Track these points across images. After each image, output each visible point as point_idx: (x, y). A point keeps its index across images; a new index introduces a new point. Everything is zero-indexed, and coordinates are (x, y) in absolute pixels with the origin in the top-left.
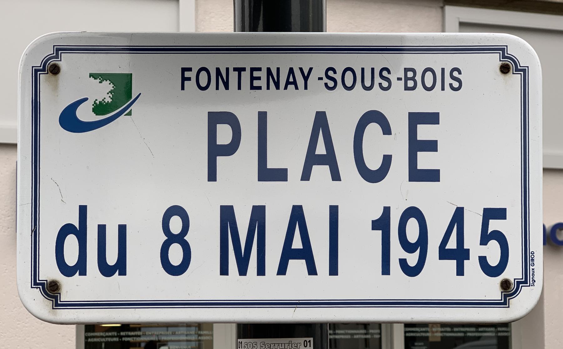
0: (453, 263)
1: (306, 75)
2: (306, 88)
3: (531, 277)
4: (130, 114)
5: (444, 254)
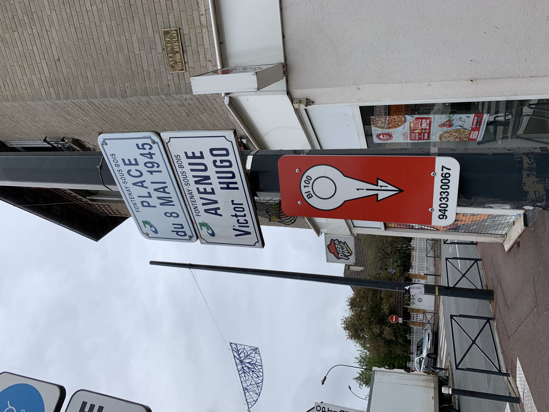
5: (152, 158)
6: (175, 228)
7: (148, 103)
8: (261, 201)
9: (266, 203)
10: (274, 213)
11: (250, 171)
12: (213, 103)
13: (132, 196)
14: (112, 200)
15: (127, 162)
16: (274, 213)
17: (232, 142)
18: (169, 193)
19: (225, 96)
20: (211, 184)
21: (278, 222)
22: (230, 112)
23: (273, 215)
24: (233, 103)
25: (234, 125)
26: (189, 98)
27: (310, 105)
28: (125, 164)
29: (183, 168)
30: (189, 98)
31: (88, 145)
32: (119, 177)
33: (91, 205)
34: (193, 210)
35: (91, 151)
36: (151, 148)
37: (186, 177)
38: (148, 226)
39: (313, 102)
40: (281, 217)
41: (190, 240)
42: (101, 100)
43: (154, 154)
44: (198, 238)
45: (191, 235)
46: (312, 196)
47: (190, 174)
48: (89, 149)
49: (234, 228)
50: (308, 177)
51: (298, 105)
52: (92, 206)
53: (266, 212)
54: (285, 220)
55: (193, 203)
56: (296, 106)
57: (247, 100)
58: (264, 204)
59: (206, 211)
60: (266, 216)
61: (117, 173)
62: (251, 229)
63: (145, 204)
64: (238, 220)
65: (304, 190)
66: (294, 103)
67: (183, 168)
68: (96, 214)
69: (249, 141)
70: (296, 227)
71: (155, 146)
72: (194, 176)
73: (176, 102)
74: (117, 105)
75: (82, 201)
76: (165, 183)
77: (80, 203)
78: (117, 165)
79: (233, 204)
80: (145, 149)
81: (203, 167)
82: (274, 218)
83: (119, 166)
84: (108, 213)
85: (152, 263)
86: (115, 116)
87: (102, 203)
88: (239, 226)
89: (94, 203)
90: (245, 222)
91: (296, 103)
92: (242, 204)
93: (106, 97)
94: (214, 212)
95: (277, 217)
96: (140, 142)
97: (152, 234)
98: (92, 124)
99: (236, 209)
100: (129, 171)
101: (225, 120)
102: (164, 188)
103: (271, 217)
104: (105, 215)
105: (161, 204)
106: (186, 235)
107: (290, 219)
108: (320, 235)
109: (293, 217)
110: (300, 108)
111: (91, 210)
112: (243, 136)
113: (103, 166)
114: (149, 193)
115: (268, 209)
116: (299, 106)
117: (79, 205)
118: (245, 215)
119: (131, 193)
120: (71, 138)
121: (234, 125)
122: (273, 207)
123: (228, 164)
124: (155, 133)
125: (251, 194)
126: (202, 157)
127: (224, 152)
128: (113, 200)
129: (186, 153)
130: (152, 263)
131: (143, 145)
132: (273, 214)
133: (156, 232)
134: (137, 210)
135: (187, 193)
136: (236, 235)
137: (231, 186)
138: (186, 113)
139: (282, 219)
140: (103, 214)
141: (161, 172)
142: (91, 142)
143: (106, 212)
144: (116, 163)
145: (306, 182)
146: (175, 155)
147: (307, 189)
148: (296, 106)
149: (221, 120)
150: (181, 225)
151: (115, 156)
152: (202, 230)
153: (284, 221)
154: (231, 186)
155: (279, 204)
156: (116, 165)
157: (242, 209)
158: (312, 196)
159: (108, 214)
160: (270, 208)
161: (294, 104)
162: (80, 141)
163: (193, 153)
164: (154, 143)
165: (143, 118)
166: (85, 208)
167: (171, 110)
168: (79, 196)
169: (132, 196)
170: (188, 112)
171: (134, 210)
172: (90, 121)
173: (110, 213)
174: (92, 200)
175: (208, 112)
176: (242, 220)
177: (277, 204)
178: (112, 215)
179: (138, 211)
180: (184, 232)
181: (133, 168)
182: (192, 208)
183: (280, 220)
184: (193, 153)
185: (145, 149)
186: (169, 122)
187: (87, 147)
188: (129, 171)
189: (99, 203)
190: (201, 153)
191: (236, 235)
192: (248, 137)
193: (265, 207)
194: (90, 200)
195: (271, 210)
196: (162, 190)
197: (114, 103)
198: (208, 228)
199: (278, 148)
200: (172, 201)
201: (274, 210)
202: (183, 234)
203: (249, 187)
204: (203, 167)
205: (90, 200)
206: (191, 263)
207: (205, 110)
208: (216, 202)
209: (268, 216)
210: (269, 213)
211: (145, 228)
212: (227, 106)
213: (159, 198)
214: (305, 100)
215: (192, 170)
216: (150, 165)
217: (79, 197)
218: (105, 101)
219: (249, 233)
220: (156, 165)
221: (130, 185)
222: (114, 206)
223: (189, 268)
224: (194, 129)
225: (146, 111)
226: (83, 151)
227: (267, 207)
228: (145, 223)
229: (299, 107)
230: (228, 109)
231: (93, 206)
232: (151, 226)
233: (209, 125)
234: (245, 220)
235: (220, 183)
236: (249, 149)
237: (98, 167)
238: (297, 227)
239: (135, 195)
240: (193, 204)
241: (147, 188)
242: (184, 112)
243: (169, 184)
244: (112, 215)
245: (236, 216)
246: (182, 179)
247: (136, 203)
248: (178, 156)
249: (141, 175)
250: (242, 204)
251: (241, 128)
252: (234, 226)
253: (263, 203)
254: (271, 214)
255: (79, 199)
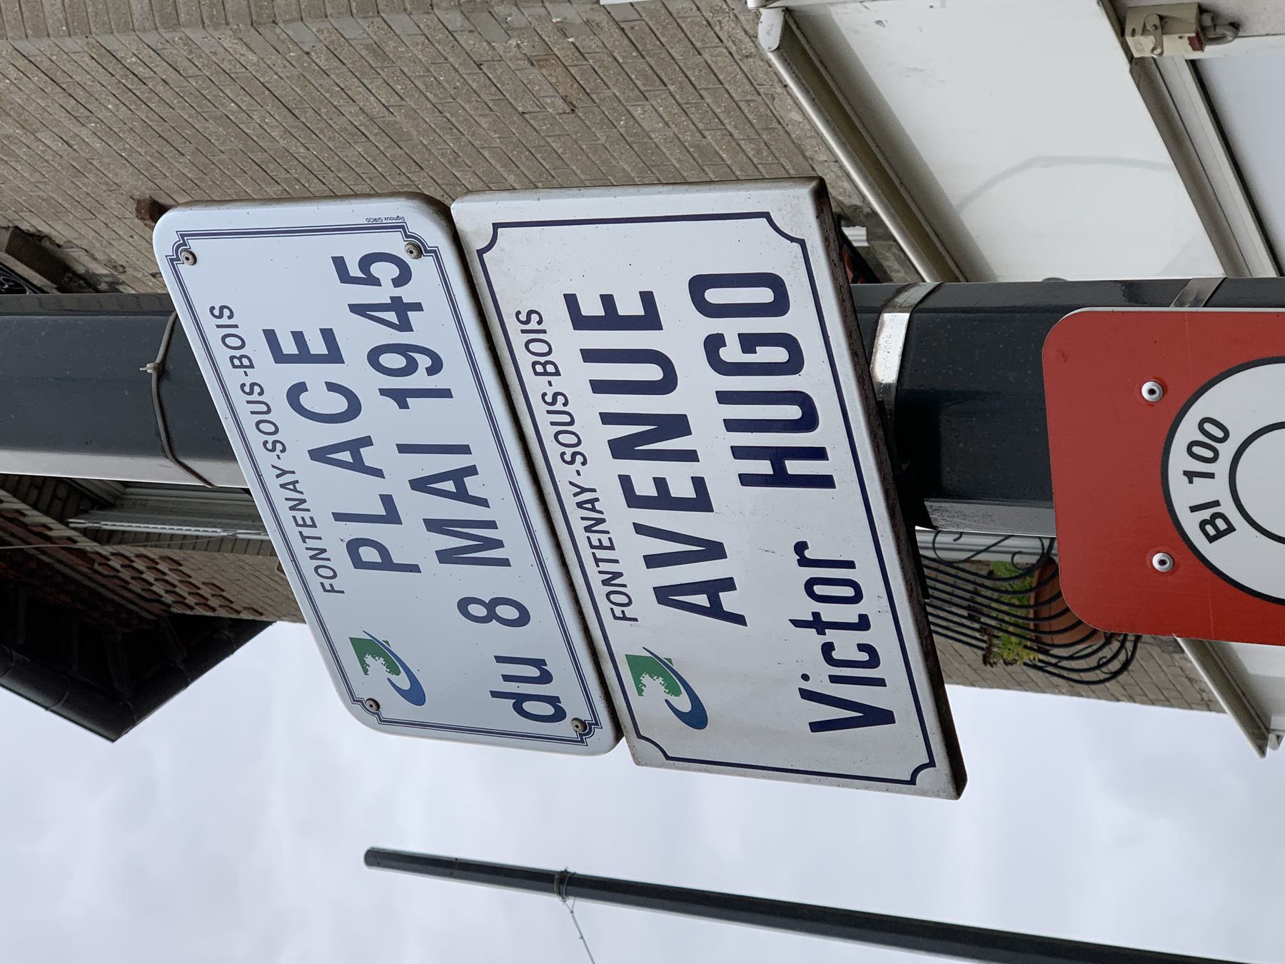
0: (412, 315)
1: (580, 490)
2: (594, 490)
3: (394, 221)
4: (669, 660)
5: (405, 326)
6: (507, 678)
7: (377, 49)
8: (943, 555)
9: (966, 566)
10: (1013, 620)
11: (894, 390)
12: (698, 45)
13: (306, 515)
14: (192, 537)
15: (289, 347)
16: (1013, 620)
17: (802, 243)
18: (483, 502)
19: (764, 6)
20: (691, 456)
21: (1034, 667)
22: (786, 86)
23: (1007, 632)
24: (803, 41)
25: (804, 156)
26: (578, 21)
27: (1219, 39)
28: (279, 357)
29: (557, 373)
30: (578, 21)
31: (85, 259)
32: (248, 422)
33: (93, 556)
34: (600, 591)
35: (97, 291)
36: (404, 277)
37: (567, 419)
38: (376, 664)
39: (1235, 26)
40: (1047, 639)
41: (582, 741)
42: (152, 38)
43: (417, 307)
44: (619, 733)
45: (586, 716)
46: (1231, 529)
47: (586, 407)
48: (88, 283)
49: (807, 686)
50: (1208, 426)
51: (1152, 38)
52: (94, 561)
53: (965, 613)
54: (1071, 658)
55: (601, 554)
56: (1143, 46)
57: (879, 22)
58: (953, 571)
59: (665, 595)
60: (969, 632)
61: (239, 399)
62: (893, 696)
63: (368, 554)
64: (827, 649)
65: (1183, 495)
66: (1128, 30)
67: (557, 373)
68: (112, 601)
69: (880, 238)
70: (1131, 699)
71: (422, 268)
72: (608, 418)
73: (513, 42)
74: (226, 66)
75: (49, 539)
76: (465, 450)
77: (37, 549)
78: (240, 358)
79: (804, 562)
80: (375, 282)
81: (653, 373)
82: (1009, 646)
83: (251, 366)
84: (168, 599)
85: (377, 858)
86: (215, 119)
87: (142, 550)
88: (834, 679)
89: (106, 550)
90: (864, 657)
91: (1139, 30)
92: (850, 565)
93: (173, 22)
94: (702, 600)
95: (1029, 644)
96: (354, 249)
97: (395, 706)
98: (107, 160)
99: (819, 590)
100: (295, 392)
101: (757, 127)
102: (458, 476)
103: (996, 641)
104: (155, 608)
105: (446, 556)
106: (559, 715)
107: (1100, 654)
108: (1269, 750)
109: (1115, 645)
110: (1161, 54)
111: (92, 585)
112: (848, 212)
113: (170, 366)
114: (387, 500)
115: (979, 599)
116: (1159, 44)
117: (31, 557)
118: (863, 623)
119: (304, 501)
120: (7, 228)
121: (804, 156)
122: (1005, 585)
123: (779, 355)
124: (423, 206)
125: (898, 508)
126: (650, 319)
127: (764, 295)
128: (197, 537)
129: (571, 301)
130: (377, 858)
131: (366, 262)
132: (1004, 626)
133: (415, 695)
134: (327, 583)
135: (570, 502)
136: (817, 727)
137: (794, 467)
138: (564, 99)
139: (1055, 651)
140: (147, 605)
141: (446, 393)
142: (97, 245)
143: (162, 593)
144: (238, 353)
145: (1196, 450)
146: (518, 313)
147: (1203, 491)
148: (1143, 46)
149: (736, 127)
150: (539, 663)
151: (231, 317)
152: (640, 692)
153: (1064, 663)
154: (794, 467)
155: (1036, 574)
156: (237, 362)
157: (848, 592)
158: (1231, 529)
159: (169, 606)
160: (988, 593)
161: (1129, 39)
162: (46, 244)
163: (608, 301)
164: (420, 254)
165: (350, 128)
166: (63, 575)
167: (488, 82)
168: (35, 513)
169: (306, 515)
170: (574, 94)
171: (314, 581)
172: (98, 145)
173: (181, 601)
174: (96, 535)
175: (672, 88)
176: (846, 644)
177: (1029, 570)
178: (189, 612)
179: (333, 590)
180: (553, 701)
181: (315, 375)
182: (596, 579)
183: (1041, 657)
184: (608, 301)
185: (375, 282)
186: (477, 143)
187: (81, 270)
188: (295, 392)
189: (152, 553)
190: (647, 298)
191: (817, 727)
192: (875, 214)
193: (959, 583)
194: (85, 532)
195: (994, 605)
196: (449, 486)
197: (215, 53)
198: (674, 680)
199: (1037, 275)
200: (498, 544)
201: (1013, 605)
202: (548, 710)
203: (890, 477)
204: (653, 373)
205: (85, 532)
206: (572, 870)
207: (658, 82)
208: (714, 551)
209: (977, 635)
210: (984, 619)
211: (366, 672)
212: (773, 58)
213: (434, 526)
214: (1191, 15)
215: (600, 387)
216: (394, 361)
217: (35, 517)
218: (168, 46)
219: (884, 717)
220: (424, 361)
221: (296, 459)
222: (199, 567)
223: (560, 893)
224: (603, 180)
225: (367, 94)
226: (62, 289)
227: (970, 587)
228: (366, 647)
229: (1159, 51)
230: (777, 74)
231: (100, 564)
232: (394, 664)
233: (673, 156)
234: (862, 647)
235: (739, 452)
236: (878, 276)
237: (149, 368)
238: (1137, 698)
239: (320, 507)
240: (597, 561)
241: (378, 473)
242: (551, 92)
243: (484, 456)
244: (191, 608)
245: (817, 624)
246: (548, 432)
247: (324, 551)
248: (535, 318)
249: (354, 408)
250: (850, 565)
251: (842, 167)
252: (805, 677)
253: (950, 564)
254: (993, 623)
255: (35, 529)
